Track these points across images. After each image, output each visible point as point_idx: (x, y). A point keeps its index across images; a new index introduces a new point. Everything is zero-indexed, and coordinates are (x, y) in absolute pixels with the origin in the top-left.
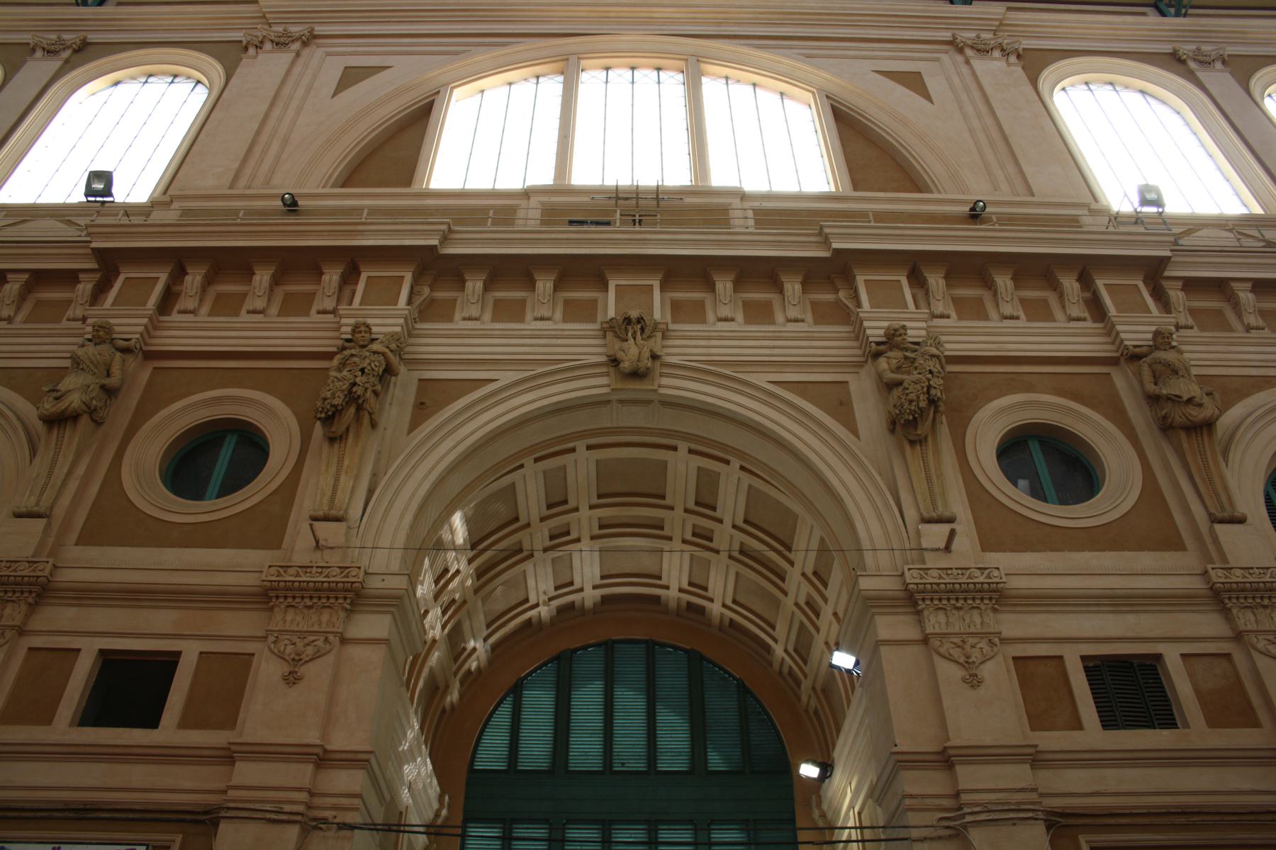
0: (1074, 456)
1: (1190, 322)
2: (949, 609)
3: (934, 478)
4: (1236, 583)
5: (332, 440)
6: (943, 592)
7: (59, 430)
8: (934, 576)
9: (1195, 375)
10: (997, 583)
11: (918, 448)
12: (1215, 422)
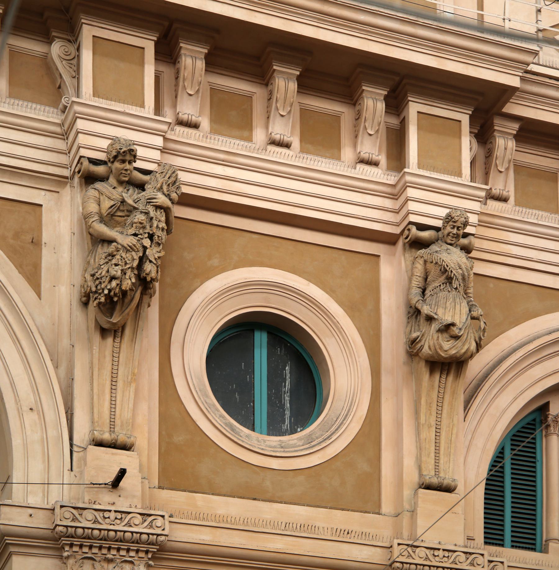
5: (104, 332)
7: (440, 377)
8: (89, 519)
10: (158, 535)
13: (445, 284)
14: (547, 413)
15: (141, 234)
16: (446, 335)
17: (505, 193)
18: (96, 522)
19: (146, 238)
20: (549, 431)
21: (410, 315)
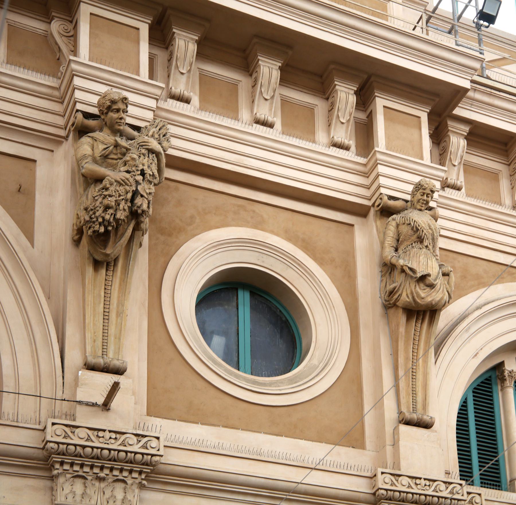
0: (284, 319)
1: (461, 181)
2: (89, 478)
3: (113, 316)
4: (400, 492)
6: (87, 457)
8: (404, 484)
9: (440, 248)
10: (153, 455)
11: (103, 271)
12: (440, 310)
13: (416, 243)
14: (504, 368)
15: (134, 172)
16: (422, 285)
17: (459, 183)
18: (89, 441)
19: (138, 175)
20: (505, 384)
21: (383, 273)
